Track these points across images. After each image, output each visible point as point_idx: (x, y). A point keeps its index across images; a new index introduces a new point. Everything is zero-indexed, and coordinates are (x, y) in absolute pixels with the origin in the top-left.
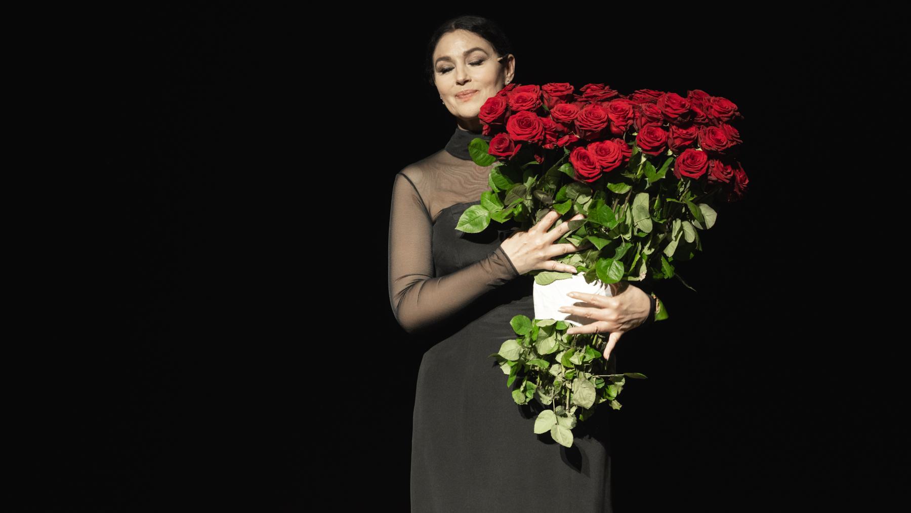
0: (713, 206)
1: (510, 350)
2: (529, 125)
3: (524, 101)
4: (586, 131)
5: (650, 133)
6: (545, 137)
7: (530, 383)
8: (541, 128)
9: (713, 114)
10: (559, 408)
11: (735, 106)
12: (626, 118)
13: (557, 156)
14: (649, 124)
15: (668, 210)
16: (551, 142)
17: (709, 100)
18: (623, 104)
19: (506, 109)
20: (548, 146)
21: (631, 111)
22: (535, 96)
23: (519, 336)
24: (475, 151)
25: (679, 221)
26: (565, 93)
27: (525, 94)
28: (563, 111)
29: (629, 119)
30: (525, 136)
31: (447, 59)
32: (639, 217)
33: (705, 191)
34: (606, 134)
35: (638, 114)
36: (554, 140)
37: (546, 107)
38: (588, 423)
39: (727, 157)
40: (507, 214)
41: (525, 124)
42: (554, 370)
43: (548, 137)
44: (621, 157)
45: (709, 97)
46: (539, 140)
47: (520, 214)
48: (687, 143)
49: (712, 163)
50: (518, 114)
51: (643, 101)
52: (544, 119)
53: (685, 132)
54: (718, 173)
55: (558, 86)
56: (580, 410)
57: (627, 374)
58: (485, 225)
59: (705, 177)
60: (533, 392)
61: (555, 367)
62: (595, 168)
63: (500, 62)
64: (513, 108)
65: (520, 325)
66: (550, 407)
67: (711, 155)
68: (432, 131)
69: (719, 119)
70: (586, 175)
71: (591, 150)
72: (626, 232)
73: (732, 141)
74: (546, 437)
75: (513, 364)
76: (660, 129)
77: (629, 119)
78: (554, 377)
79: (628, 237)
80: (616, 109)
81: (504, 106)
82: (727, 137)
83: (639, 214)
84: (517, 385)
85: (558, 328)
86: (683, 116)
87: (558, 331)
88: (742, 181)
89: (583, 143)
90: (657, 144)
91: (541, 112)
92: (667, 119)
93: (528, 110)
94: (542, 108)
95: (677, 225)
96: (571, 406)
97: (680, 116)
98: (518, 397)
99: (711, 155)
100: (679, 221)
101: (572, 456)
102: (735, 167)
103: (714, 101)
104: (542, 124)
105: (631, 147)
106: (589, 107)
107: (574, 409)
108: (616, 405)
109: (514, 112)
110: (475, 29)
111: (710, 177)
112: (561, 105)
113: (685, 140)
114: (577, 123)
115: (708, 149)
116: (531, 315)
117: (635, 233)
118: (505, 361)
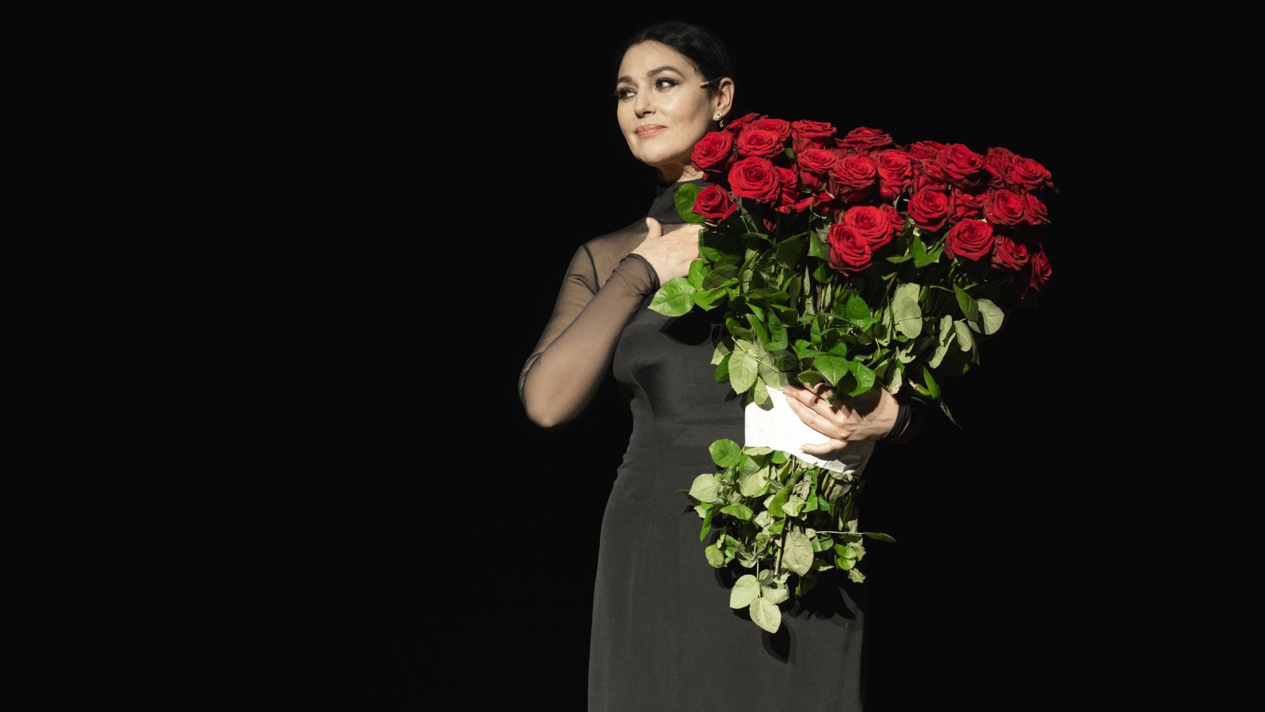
0: (998, 303)
1: (705, 488)
2: (759, 177)
3: (760, 142)
4: (842, 186)
5: (929, 199)
6: (780, 195)
7: (730, 538)
8: (776, 183)
9: (1013, 178)
10: (765, 574)
11: (1048, 173)
12: (901, 176)
13: (803, 224)
14: (928, 187)
15: (934, 308)
16: (787, 204)
17: (1010, 159)
18: (898, 157)
19: (730, 153)
20: (782, 209)
21: (909, 168)
22: (775, 138)
23: (721, 470)
24: (684, 200)
25: (948, 318)
26: (820, 134)
27: (765, 134)
28: (815, 158)
29: (906, 177)
30: (753, 191)
31: (627, 80)
32: (904, 315)
33: (988, 280)
34: (872, 196)
35: (917, 172)
36: (792, 201)
37: (790, 153)
38: (813, 595)
39: (1019, 233)
40: (718, 296)
41: (755, 175)
42: (762, 519)
43: (784, 196)
44: (891, 231)
45: (1011, 154)
46: (772, 200)
47: (737, 298)
48: (972, 213)
49: (999, 240)
50: (746, 160)
51: (924, 155)
52: (783, 170)
53: (971, 198)
54: (1005, 255)
55: (816, 126)
56: (793, 580)
57: (868, 533)
58: (689, 307)
59: (988, 258)
60: (735, 550)
61: (763, 514)
62: (862, 254)
63: (703, 87)
64: (741, 151)
65: (724, 453)
66: (752, 571)
67: (998, 230)
68: (638, 193)
69: (1021, 186)
70: (852, 263)
71: (847, 218)
72: (882, 336)
73: (1036, 219)
74: (744, 613)
75: (709, 507)
76: (942, 195)
77: (906, 177)
78: (761, 529)
79: (885, 343)
80: (888, 162)
81: (727, 149)
82: (1030, 210)
83: (905, 310)
84: (713, 539)
85: (774, 460)
86: (971, 177)
87: (771, 465)
88: (1043, 272)
89: (839, 204)
90: (936, 215)
91: (782, 161)
92: (947, 179)
93: (763, 156)
94: (784, 154)
95: (946, 323)
96: (781, 571)
97: (967, 177)
98: (714, 556)
99: (998, 230)
100: (948, 318)
101: (779, 643)
102: (1032, 251)
103: (1018, 161)
104: (777, 178)
105: (904, 217)
106: (852, 158)
107: (785, 577)
108: (858, 577)
109: (741, 157)
110: (671, 43)
111: (994, 259)
112: (815, 150)
113: (971, 209)
114: (831, 174)
115: (996, 222)
116: (740, 440)
117: (895, 337)
118: (698, 503)
